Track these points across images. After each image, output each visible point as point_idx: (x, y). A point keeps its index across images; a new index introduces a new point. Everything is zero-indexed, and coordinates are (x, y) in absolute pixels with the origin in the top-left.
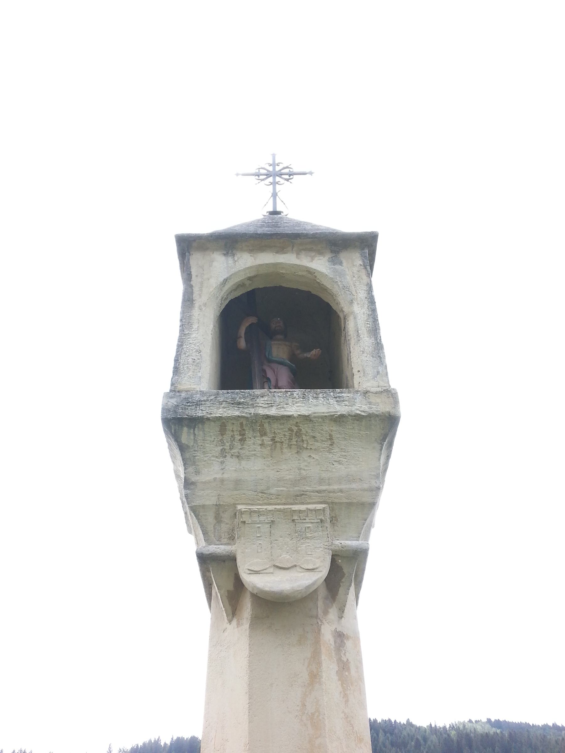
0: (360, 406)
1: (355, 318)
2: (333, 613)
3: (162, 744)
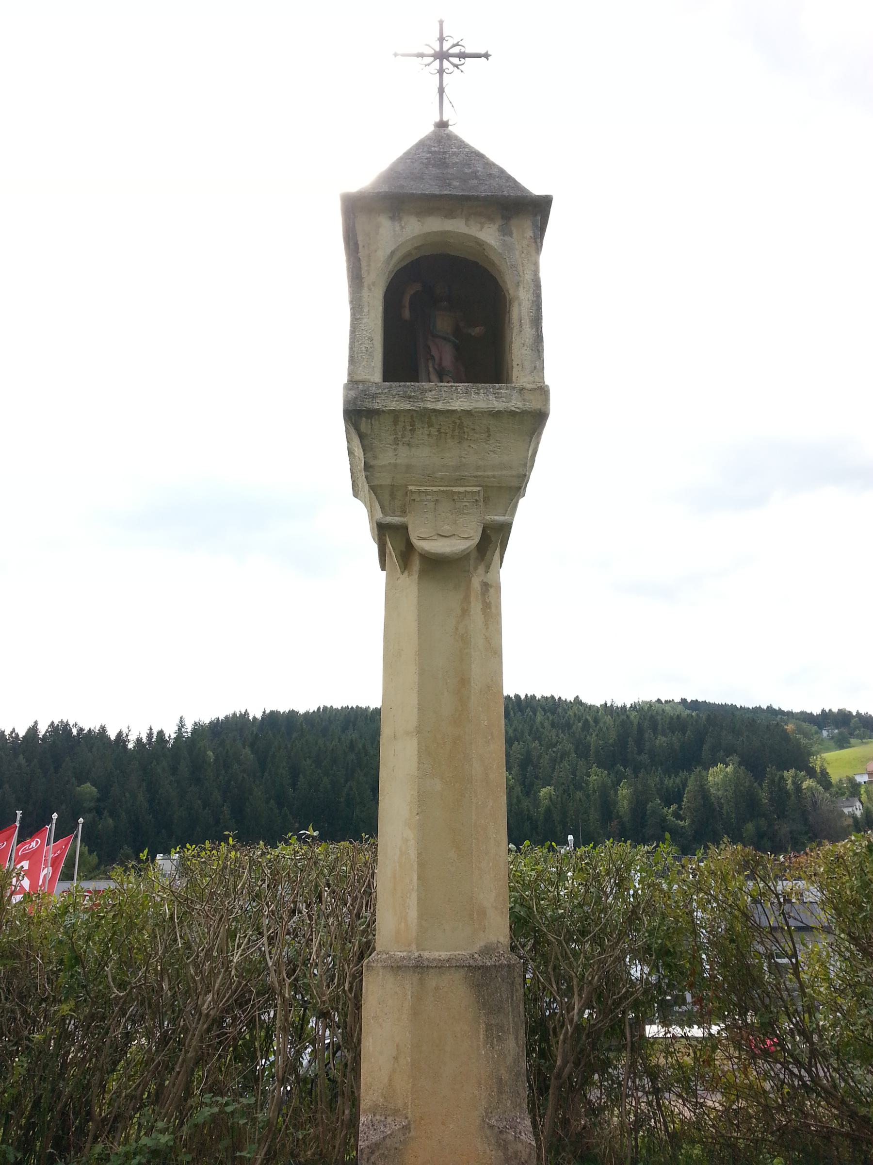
0: (515, 403)
1: (520, 305)
2: (481, 569)
3: (251, 718)
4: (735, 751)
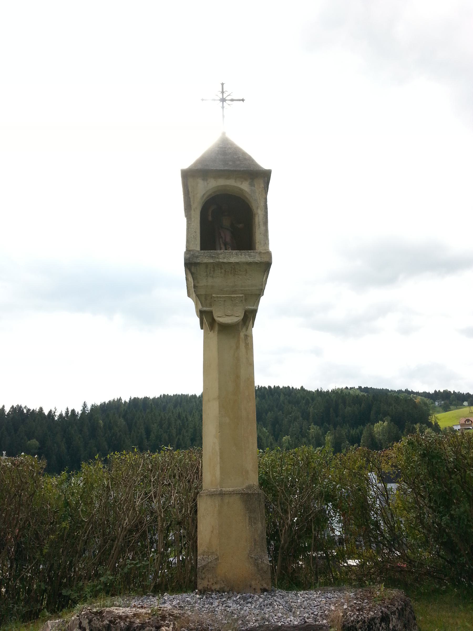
0: (257, 259)
1: (258, 216)
2: (244, 329)
3: (123, 402)
4: (389, 415)
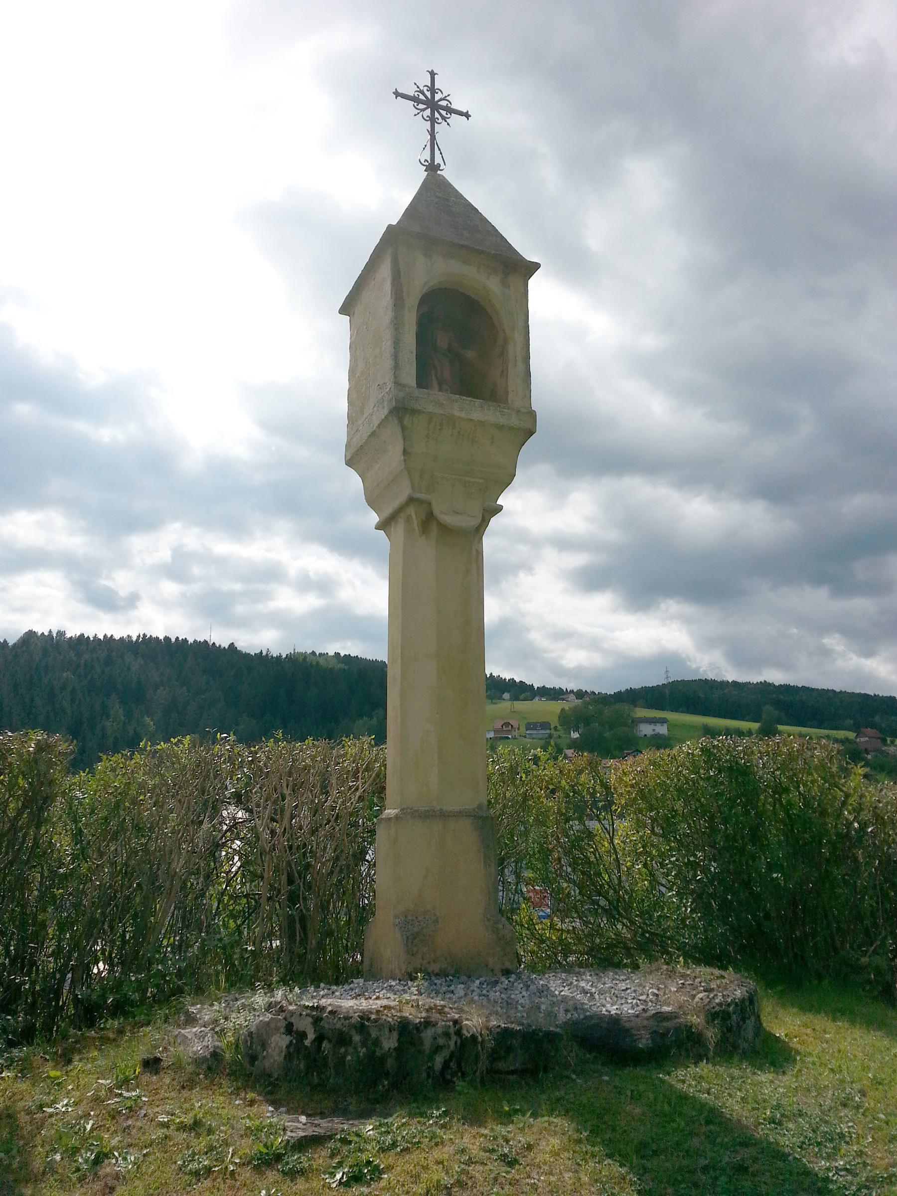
0: (514, 421)
